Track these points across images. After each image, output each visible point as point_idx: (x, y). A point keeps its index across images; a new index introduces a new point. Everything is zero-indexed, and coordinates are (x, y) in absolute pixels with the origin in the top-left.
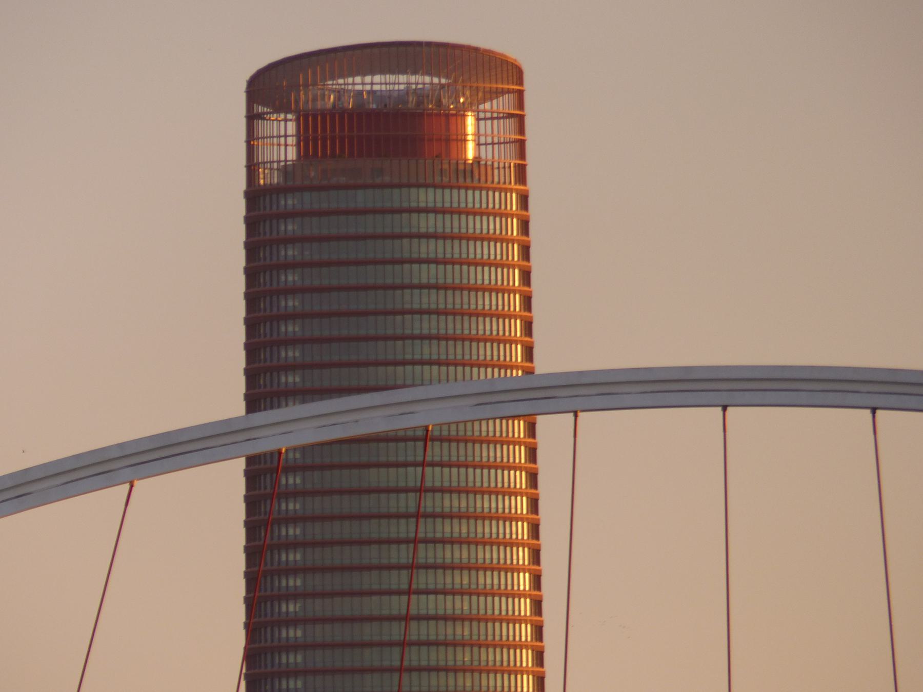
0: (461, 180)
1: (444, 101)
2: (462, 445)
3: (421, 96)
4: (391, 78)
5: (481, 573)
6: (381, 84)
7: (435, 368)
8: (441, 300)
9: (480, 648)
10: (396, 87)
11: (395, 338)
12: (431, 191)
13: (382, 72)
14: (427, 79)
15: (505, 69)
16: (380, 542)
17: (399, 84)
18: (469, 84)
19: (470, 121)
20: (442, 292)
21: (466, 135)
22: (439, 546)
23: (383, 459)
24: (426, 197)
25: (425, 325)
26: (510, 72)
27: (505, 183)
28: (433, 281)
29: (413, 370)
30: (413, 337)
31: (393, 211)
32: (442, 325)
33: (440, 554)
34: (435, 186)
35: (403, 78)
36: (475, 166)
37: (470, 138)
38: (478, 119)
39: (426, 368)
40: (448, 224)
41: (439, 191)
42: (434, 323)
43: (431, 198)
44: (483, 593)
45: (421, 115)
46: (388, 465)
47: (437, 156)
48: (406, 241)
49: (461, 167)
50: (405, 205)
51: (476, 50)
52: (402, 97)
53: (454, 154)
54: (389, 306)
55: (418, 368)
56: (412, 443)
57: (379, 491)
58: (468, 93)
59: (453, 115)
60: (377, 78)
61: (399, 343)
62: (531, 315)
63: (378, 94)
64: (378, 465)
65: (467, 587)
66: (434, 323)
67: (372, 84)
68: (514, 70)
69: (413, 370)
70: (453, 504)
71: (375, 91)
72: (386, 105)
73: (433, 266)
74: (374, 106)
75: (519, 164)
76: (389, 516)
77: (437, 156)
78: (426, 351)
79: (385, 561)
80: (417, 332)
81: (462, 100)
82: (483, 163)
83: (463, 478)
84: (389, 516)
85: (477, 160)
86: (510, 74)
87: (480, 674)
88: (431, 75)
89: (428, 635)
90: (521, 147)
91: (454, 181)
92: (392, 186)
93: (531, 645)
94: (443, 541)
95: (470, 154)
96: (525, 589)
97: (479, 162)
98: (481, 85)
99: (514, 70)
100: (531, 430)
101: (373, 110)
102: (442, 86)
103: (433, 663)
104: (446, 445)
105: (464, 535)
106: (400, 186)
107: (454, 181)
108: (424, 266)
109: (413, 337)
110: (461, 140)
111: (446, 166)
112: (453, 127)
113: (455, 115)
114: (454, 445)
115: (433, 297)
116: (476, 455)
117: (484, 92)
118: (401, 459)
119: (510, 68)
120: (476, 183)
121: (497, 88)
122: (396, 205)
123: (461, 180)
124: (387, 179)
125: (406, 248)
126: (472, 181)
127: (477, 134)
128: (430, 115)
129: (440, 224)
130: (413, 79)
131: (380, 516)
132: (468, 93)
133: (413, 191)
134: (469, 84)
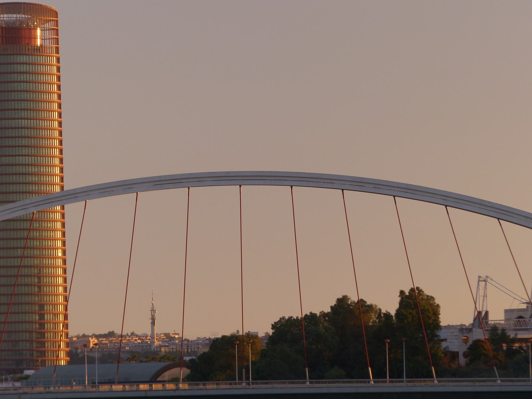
0: (36, 52)
1: (30, 24)
2: (34, 66)
3: (21, 22)
4: (10, 15)
5: (42, 167)
6: (7, 17)
7: (26, 120)
8: (29, 133)
9: (38, 74)
10: (12, 19)
11: (12, 110)
12: (25, 56)
13: (7, 14)
14: (23, 16)
15: (51, 12)
16: (6, 184)
17: (13, 17)
18: (38, 18)
19: (39, 31)
20: (29, 130)
21: (37, 36)
22: (28, 185)
23: (7, 154)
24: (24, 59)
25: (23, 105)
26: (53, 13)
27: (51, 53)
28: (25, 89)
29: (19, 158)
30: (18, 110)
31: (11, 64)
32: (29, 105)
33: (28, 188)
34: (26, 55)
35: (15, 16)
36: (41, 47)
37: (38, 37)
38: (41, 30)
39: (23, 121)
40: (31, 68)
41: (28, 56)
42: (26, 114)
43: (25, 59)
44: (44, 248)
45: (21, 29)
46: (9, 156)
47: (27, 44)
48: (15, 65)
49: (36, 48)
50: (15, 61)
51: (41, 5)
52: (14, 22)
53: (33, 43)
54: (9, 61)
55: (20, 121)
56: (17, 83)
57: (6, 165)
58: (38, 21)
59: (32, 29)
60: (5, 16)
61: (13, 102)
62: (68, 321)
63: (6, 21)
64: (6, 156)
65: (37, 181)
66: (26, 104)
67: (3, 17)
68: (55, 13)
69: (19, 158)
70: (36, 308)
71: (4, 20)
72: (8, 26)
73: (25, 84)
74: (4, 26)
75: (56, 47)
76: (9, 174)
77: (27, 44)
78: (23, 114)
79: (8, 190)
80: (19, 98)
81: (36, 23)
82: (43, 46)
83: (35, 124)
84: (9, 174)
85: (41, 46)
86: (53, 14)
87: (40, 148)
88: (24, 14)
89: (23, 180)
90: (57, 41)
91: (33, 53)
92: (10, 55)
93: (63, 304)
94: (29, 183)
95: (39, 42)
96: (60, 247)
97: (42, 46)
98: (43, 18)
99: (55, 13)
100: (63, 208)
101: (4, 27)
102: (29, 18)
103: (23, 144)
104: (30, 139)
105: (37, 190)
106: (13, 55)
107: (33, 53)
108: (22, 84)
109: (18, 110)
110: (36, 29)
111: (30, 47)
112: (33, 33)
113: (34, 29)
114: (32, 102)
115: (26, 95)
116: (38, 60)
117: (44, 21)
118: (14, 153)
119: (53, 12)
120: (41, 54)
121: (49, 19)
122: (12, 61)
123: (36, 52)
124: (9, 52)
125: (15, 77)
126: (40, 53)
127: (41, 36)
128: (24, 29)
129: (27, 59)
130: (18, 16)
131: (6, 174)
132: (38, 21)
133: (18, 56)
134: (38, 18)
